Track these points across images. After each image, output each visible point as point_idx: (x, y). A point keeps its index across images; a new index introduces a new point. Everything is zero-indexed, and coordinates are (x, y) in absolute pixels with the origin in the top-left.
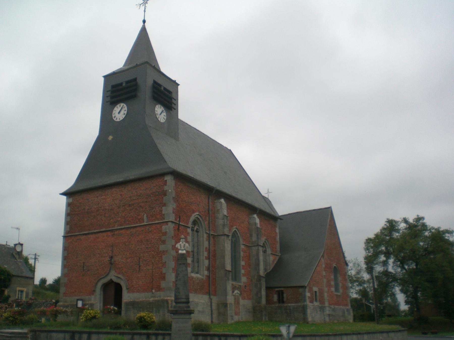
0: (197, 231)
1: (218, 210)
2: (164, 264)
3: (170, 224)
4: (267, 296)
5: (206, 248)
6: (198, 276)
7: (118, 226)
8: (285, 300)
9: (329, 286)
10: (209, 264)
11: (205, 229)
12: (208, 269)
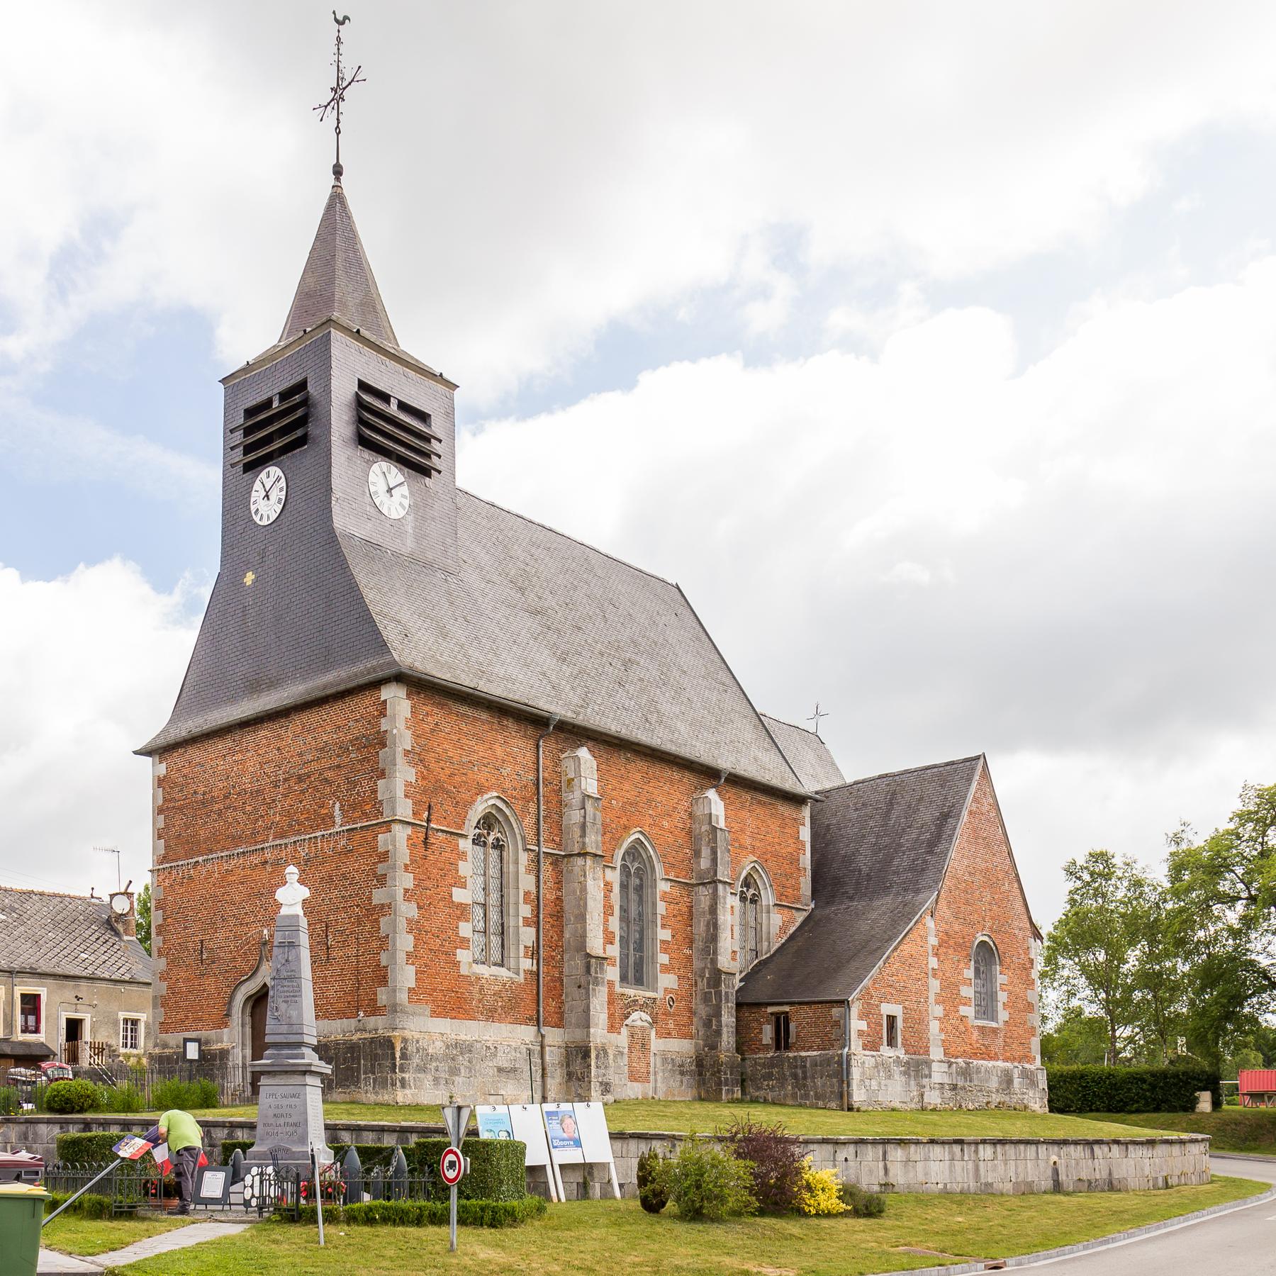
0: (498, 846)
1: (570, 781)
2: (385, 942)
3: (397, 828)
4: (740, 1029)
5: (527, 894)
6: (503, 972)
7: (275, 838)
8: (792, 1040)
9: (950, 997)
10: (538, 938)
11: (523, 838)
12: (535, 953)
